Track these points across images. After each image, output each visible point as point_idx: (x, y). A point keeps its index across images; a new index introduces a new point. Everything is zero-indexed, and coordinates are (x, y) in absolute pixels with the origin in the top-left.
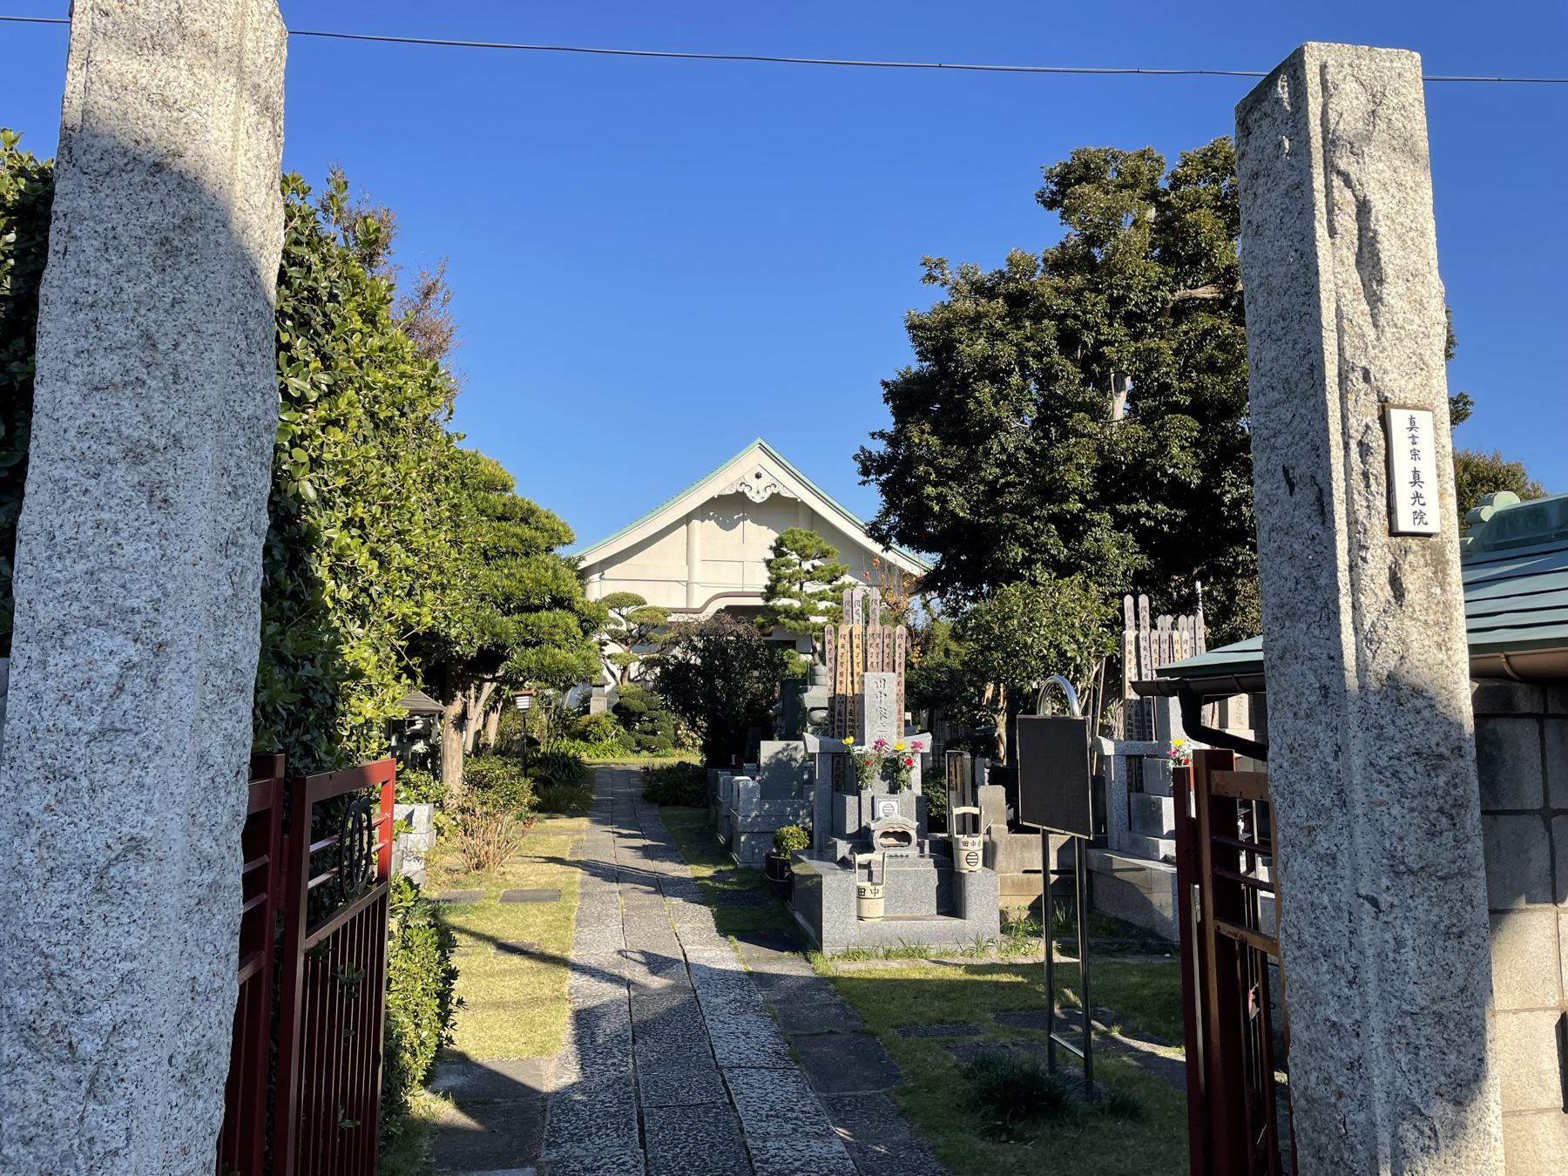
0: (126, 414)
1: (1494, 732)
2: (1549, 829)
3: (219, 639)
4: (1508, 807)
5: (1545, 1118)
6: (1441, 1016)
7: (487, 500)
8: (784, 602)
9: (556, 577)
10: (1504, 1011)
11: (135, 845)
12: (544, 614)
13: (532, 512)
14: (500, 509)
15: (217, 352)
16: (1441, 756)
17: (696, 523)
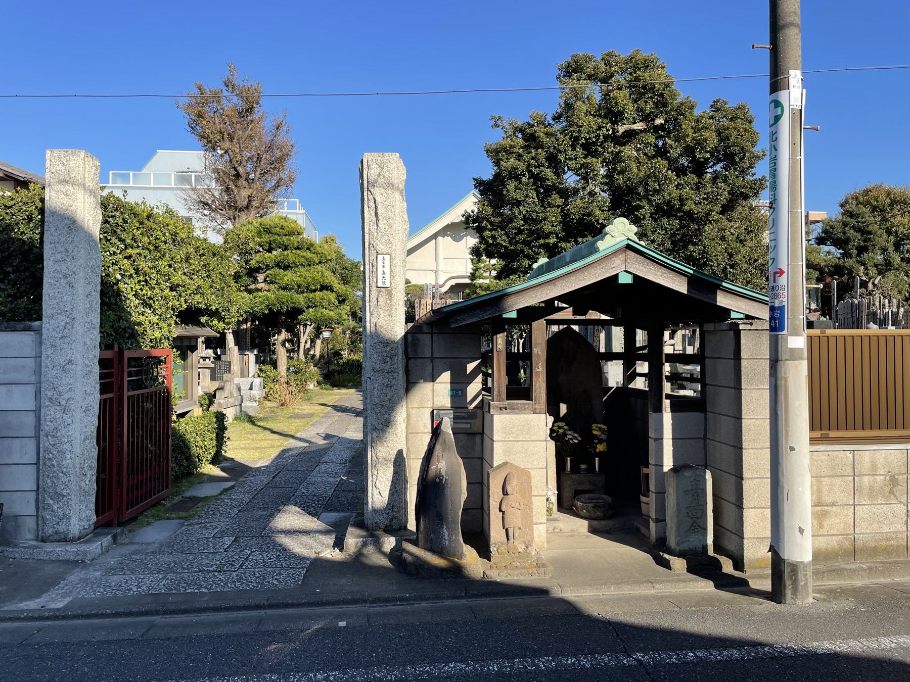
0: (63, 268)
3: (87, 317)
7: (290, 240)
8: (481, 281)
9: (322, 276)
11: (70, 361)
12: (317, 293)
13: (312, 245)
14: (296, 245)
15: (83, 251)
17: (440, 238)
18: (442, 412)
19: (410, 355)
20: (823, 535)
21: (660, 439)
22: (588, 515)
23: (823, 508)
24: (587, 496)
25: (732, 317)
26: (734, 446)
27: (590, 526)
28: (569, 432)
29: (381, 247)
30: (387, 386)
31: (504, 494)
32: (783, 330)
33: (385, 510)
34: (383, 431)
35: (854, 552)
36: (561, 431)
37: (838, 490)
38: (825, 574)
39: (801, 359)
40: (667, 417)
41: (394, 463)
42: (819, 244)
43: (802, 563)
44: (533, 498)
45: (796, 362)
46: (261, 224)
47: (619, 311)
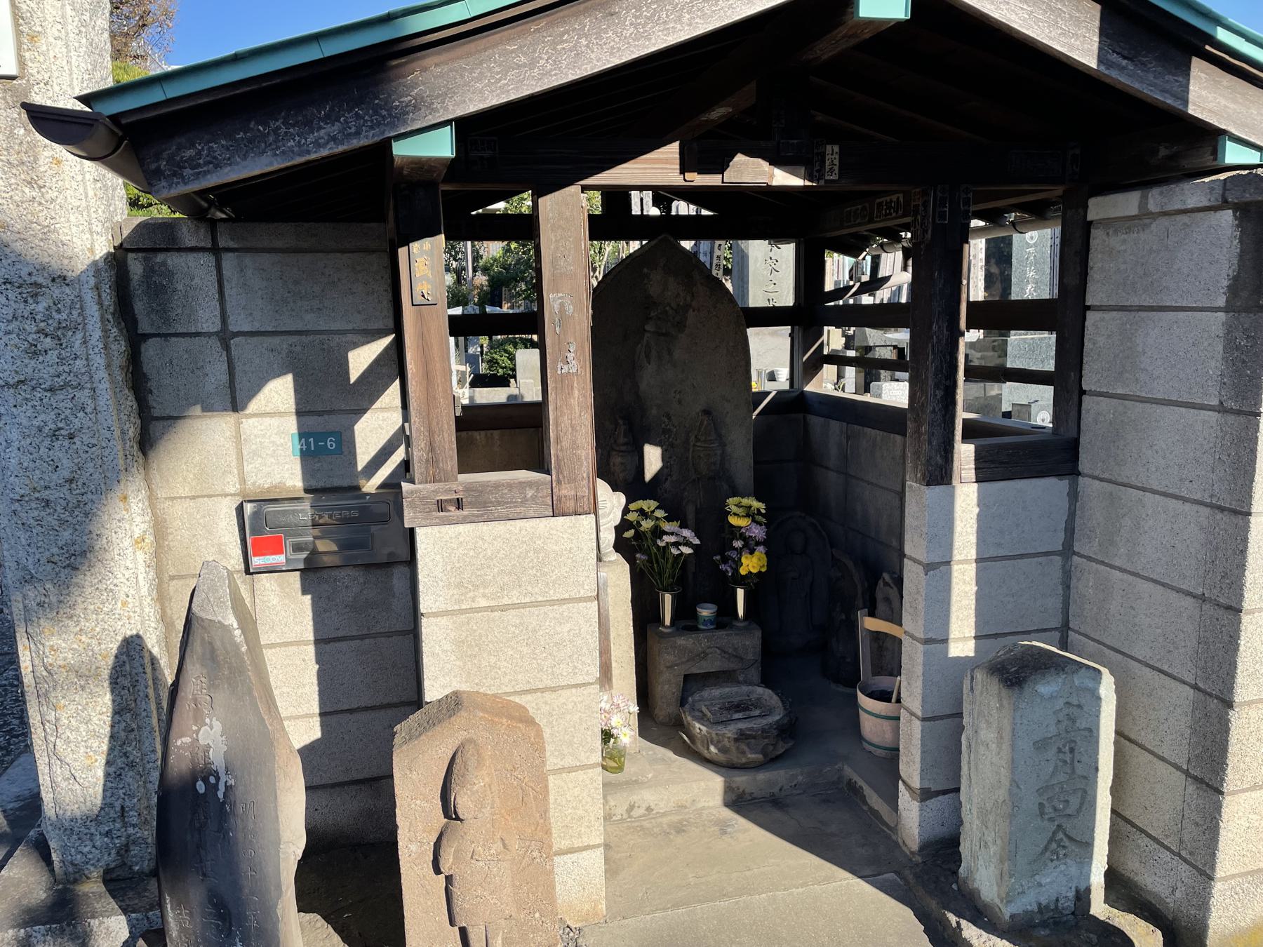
1: (164, 264)
2: (227, 348)
4: (181, 330)
6: (47, 502)
10: (1249, 703)
16: (35, 284)
18: (271, 508)
19: (144, 327)
21: (940, 566)
22: (721, 758)
24: (715, 692)
26: (1202, 598)
27: (728, 789)
28: (667, 527)
30: (54, 435)
31: (447, 814)
33: (97, 820)
34: (64, 587)
36: (647, 525)
40: (966, 495)
41: (114, 683)
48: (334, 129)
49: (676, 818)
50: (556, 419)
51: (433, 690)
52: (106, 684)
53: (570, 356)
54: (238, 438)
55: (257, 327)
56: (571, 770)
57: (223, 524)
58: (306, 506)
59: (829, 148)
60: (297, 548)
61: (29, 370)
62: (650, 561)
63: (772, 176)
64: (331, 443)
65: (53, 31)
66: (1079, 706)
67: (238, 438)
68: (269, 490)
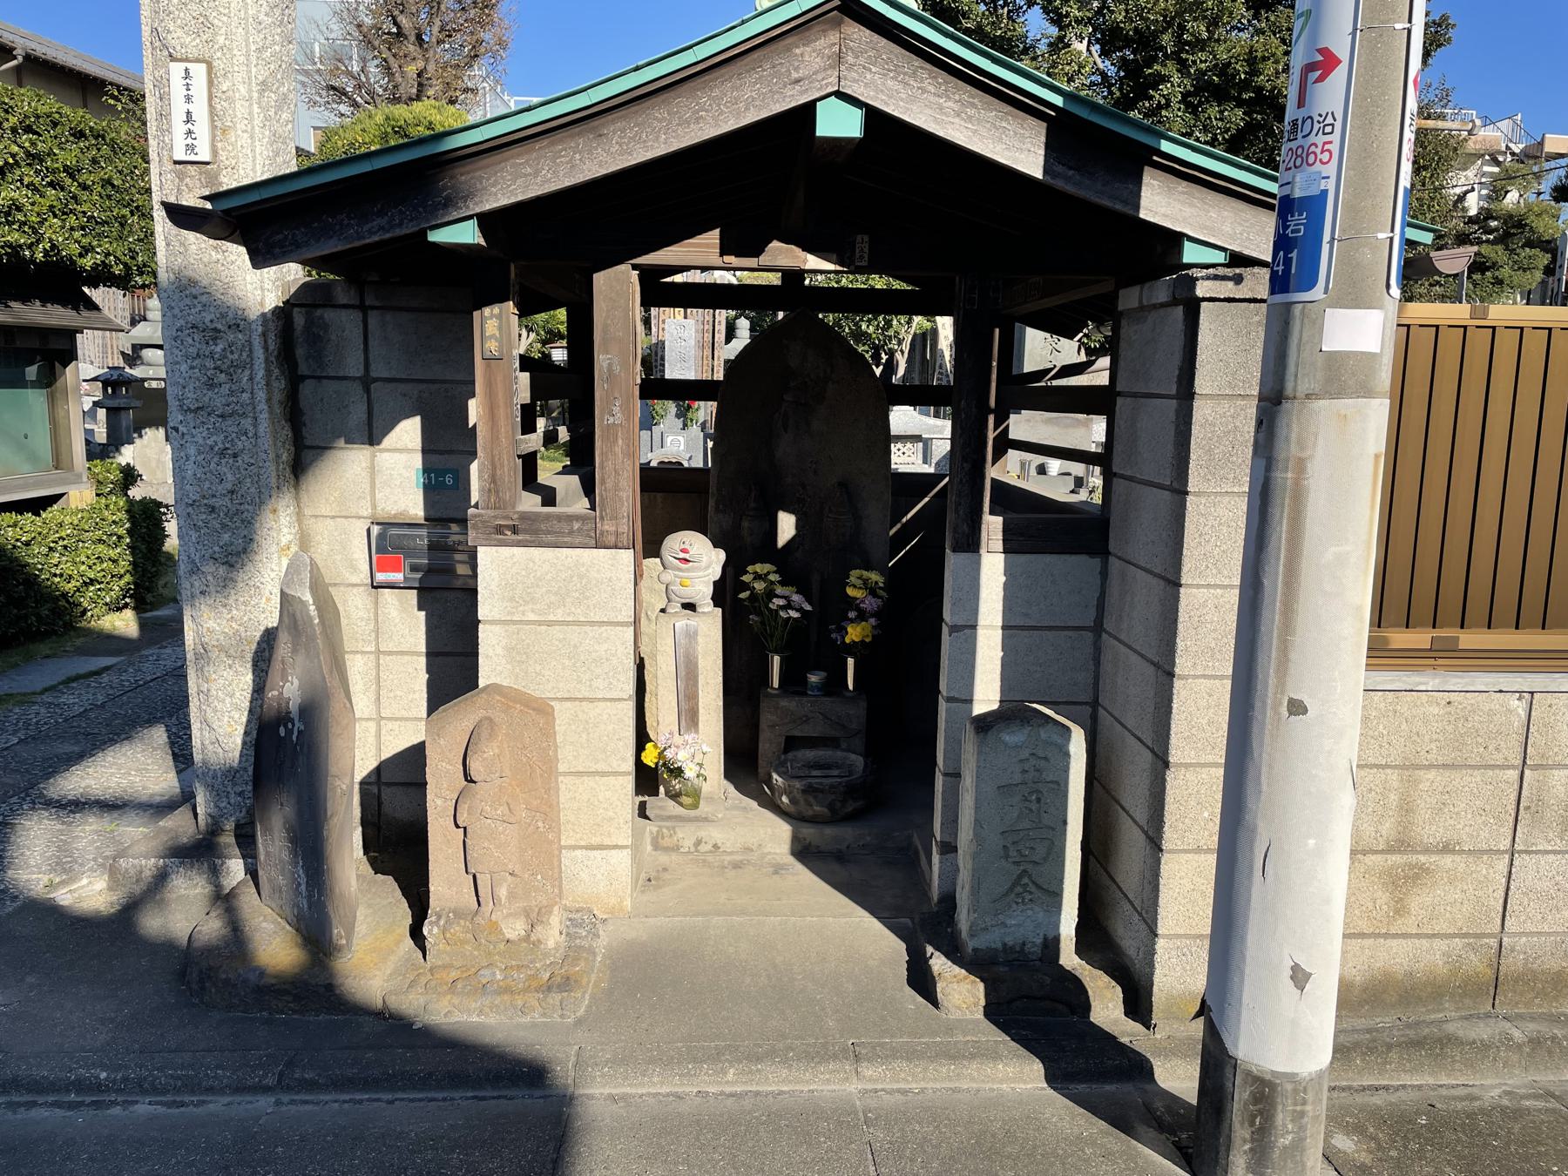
1: (321, 317)
2: (368, 391)
5: (355, 590)
10: (1187, 766)
16: (215, 330)
18: (394, 531)
19: (303, 369)
20: (1405, 936)
21: (969, 628)
22: (792, 809)
23: (1413, 858)
24: (810, 754)
25: (1186, 259)
27: (795, 839)
28: (779, 590)
29: (180, 39)
30: (222, 453)
32: (1311, 284)
35: (1494, 985)
36: (759, 586)
37: (1468, 809)
38: (1393, 1055)
39: (1367, 392)
40: (993, 566)
42: (1557, 200)
43: (1291, 1077)
44: (565, 783)
45: (1346, 405)
46: (388, 118)
47: (863, 243)
48: (383, 221)
49: (738, 858)
50: (602, 462)
51: (482, 683)
52: (249, 665)
53: (616, 409)
54: (372, 470)
55: (394, 374)
56: (604, 774)
57: (356, 542)
58: (424, 532)
59: (859, 238)
60: (414, 569)
61: (206, 399)
62: (763, 623)
63: (805, 261)
64: (449, 480)
65: (240, 126)
66: (1046, 759)
67: (372, 470)
68: (395, 516)
